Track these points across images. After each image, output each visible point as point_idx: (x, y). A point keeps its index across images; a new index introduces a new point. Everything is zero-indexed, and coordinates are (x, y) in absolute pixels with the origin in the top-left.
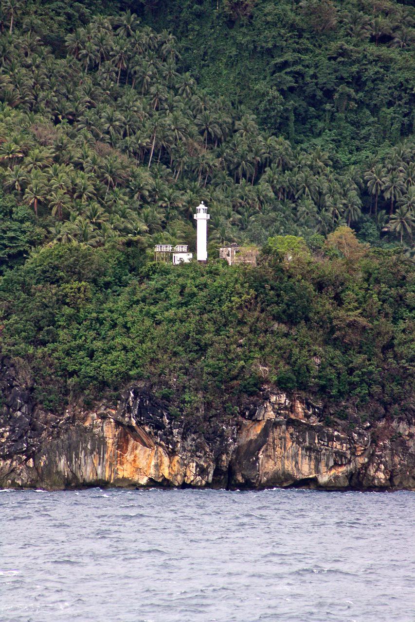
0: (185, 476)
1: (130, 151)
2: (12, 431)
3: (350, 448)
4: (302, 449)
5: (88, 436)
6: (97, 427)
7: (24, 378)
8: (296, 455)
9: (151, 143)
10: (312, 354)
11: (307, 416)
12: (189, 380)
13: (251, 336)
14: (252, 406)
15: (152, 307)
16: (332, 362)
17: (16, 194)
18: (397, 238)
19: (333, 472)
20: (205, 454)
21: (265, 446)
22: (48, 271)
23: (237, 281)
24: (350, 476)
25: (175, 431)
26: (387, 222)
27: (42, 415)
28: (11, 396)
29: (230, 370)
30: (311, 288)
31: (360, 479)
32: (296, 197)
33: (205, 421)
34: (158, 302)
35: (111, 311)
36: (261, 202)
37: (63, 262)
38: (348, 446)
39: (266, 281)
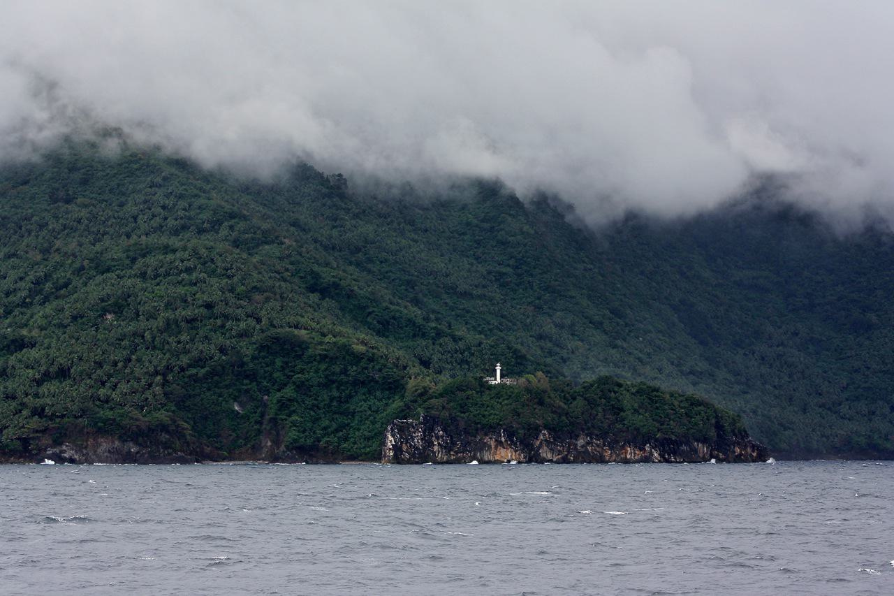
7: (462, 425)
11: (550, 438)
24: (563, 458)
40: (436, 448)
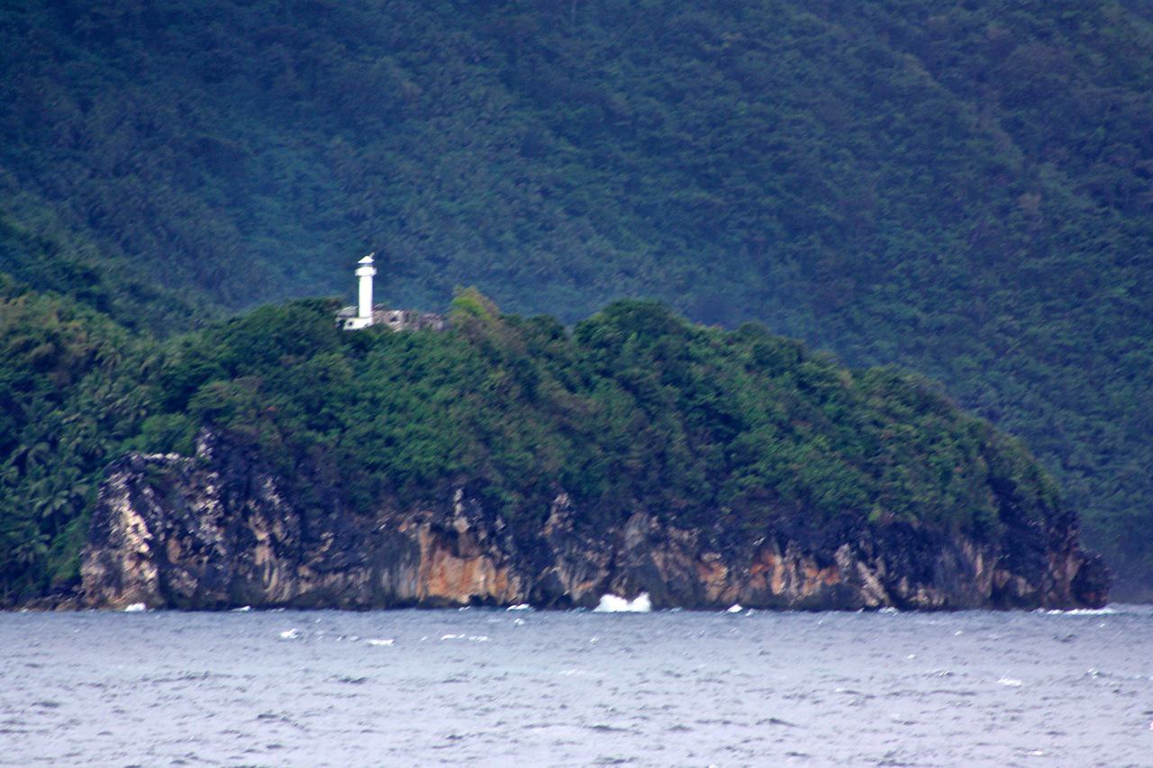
40: (263, 555)
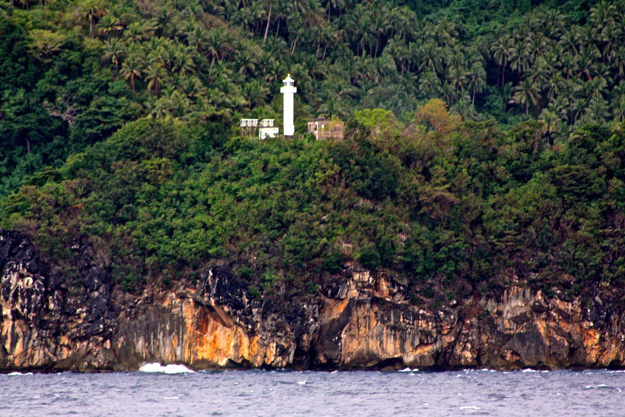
0: (265, 356)
1: (244, 24)
2: (89, 312)
3: (436, 327)
4: (387, 328)
5: (167, 316)
6: (176, 307)
7: (102, 257)
8: (380, 334)
9: (267, 14)
10: (398, 230)
11: (392, 294)
12: (270, 258)
13: (334, 212)
14: (334, 285)
15: (233, 184)
16: (418, 238)
17: (113, 69)
18: (523, 111)
19: (419, 351)
20: (286, 334)
21: (347, 326)
22: (129, 147)
23: (321, 155)
24: (436, 355)
25: (255, 311)
26: (513, 95)
27: (120, 296)
28: (89, 275)
29: (312, 248)
30: (398, 162)
31: (447, 358)
32: (420, 68)
33: (286, 299)
34: (240, 178)
35: (192, 188)
36: (382, 75)
37: (144, 137)
38: (434, 325)
39: (352, 156)
